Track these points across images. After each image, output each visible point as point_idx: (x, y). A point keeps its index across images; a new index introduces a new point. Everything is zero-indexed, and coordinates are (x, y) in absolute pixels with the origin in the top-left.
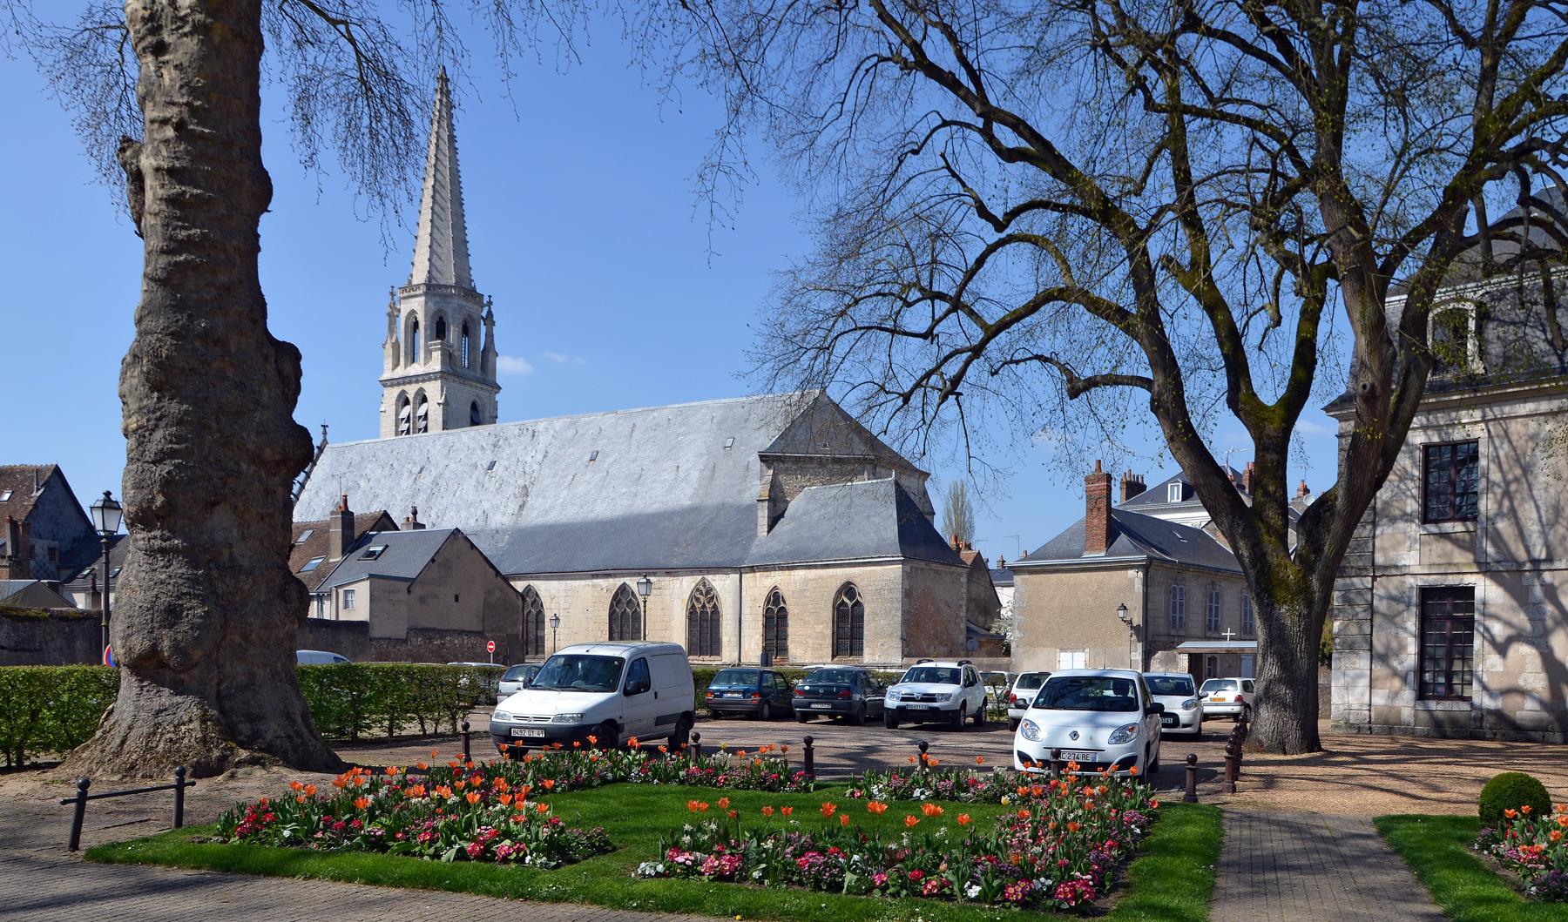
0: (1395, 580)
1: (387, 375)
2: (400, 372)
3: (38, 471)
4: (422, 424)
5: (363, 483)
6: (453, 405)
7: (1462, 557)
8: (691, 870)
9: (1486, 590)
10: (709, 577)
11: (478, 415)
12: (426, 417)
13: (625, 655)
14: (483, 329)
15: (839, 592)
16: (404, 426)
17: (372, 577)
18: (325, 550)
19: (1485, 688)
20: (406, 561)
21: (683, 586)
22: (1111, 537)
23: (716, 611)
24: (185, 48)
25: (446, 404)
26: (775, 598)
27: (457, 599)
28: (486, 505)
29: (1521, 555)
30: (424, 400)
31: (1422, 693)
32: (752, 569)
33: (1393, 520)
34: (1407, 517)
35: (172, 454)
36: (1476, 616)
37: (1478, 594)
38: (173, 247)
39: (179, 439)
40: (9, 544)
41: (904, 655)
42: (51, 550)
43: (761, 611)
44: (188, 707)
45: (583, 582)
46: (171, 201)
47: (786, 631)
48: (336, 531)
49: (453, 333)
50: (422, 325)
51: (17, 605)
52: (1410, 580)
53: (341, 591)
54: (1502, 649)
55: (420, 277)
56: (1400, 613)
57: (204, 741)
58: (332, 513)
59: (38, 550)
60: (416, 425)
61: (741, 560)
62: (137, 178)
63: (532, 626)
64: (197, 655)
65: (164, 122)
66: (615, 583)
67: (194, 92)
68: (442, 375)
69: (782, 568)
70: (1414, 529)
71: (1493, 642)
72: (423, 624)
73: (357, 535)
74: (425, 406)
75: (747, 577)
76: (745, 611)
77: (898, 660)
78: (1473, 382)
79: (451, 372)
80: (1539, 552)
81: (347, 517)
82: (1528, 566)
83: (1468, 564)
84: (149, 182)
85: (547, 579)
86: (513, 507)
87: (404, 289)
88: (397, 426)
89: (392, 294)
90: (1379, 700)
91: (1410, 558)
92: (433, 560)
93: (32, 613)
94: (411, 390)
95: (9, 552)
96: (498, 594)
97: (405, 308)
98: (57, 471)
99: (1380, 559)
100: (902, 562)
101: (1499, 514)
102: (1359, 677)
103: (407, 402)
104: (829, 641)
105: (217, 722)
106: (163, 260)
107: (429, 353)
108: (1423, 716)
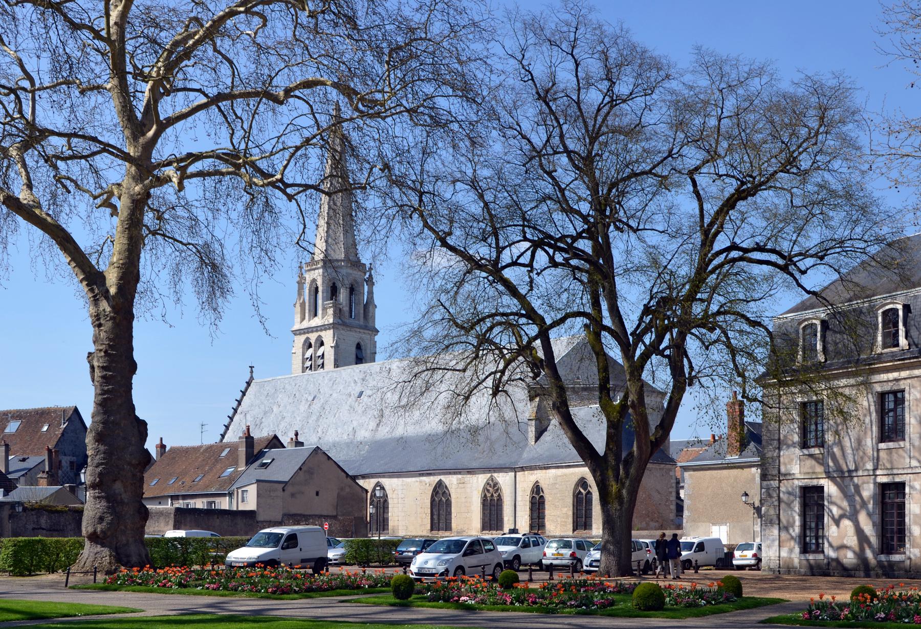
0: (790, 481)
1: (297, 326)
2: (306, 324)
3: (64, 411)
4: (320, 362)
6: (342, 347)
7: (819, 469)
8: (208, 588)
9: (831, 489)
10: (495, 475)
11: (361, 355)
12: (323, 356)
13: (285, 533)
14: (366, 288)
15: (577, 485)
16: (308, 364)
17: (258, 481)
18: (236, 463)
19: (831, 545)
20: (283, 467)
21: (480, 480)
22: (743, 446)
23: (500, 499)
24: (108, 325)
25: (336, 347)
26: (537, 489)
27: (317, 494)
28: (355, 424)
29: (845, 469)
30: (322, 344)
31: (805, 549)
32: (523, 469)
33: (788, 446)
34: (793, 445)
35: (102, 464)
36: (826, 503)
37: (826, 489)
38: (104, 392)
39: (104, 459)
40: (47, 463)
42: (72, 463)
43: (528, 499)
44: (106, 552)
45: (414, 479)
47: (544, 513)
48: (242, 450)
49: (343, 295)
50: (320, 289)
51: (51, 504)
52: (796, 482)
53: (240, 491)
54: (837, 522)
55: (319, 256)
56: (793, 502)
57: (110, 563)
58: (240, 438)
59: (64, 463)
60: (314, 364)
61: (516, 463)
62: (92, 367)
64: (109, 533)
65: (101, 350)
66: (435, 479)
67: (110, 340)
69: (541, 468)
70: (797, 451)
71: (833, 518)
72: (293, 511)
73: (256, 451)
74: (322, 349)
75: (519, 474)
76: (518, 499)
77: (571, 533)
78: (820, 366)
79: (341, 323)
80: (852, 467)
81: (249, 440)
82: (846, 474)
83: (821, 473)
84: (96, 370)
85: (390, 477)
86: (372, 425)
87: (308, 264)
88: (303, 363)
89: (301, 267)
90: (784, 554)
91: (795, 469)
92: (300, 469)
93: (59, 508)
94: (313, 337)
95: (47, 469)
96: (347, 490)
97: (309, 277)
98: (76, 410)
99: (783, 470)
101: (834, 443)
102: (773, 541)
103: (310, 346)
104: (570, 520)
105: (115, 557)
106: (100, 397)
108: (805, 562)
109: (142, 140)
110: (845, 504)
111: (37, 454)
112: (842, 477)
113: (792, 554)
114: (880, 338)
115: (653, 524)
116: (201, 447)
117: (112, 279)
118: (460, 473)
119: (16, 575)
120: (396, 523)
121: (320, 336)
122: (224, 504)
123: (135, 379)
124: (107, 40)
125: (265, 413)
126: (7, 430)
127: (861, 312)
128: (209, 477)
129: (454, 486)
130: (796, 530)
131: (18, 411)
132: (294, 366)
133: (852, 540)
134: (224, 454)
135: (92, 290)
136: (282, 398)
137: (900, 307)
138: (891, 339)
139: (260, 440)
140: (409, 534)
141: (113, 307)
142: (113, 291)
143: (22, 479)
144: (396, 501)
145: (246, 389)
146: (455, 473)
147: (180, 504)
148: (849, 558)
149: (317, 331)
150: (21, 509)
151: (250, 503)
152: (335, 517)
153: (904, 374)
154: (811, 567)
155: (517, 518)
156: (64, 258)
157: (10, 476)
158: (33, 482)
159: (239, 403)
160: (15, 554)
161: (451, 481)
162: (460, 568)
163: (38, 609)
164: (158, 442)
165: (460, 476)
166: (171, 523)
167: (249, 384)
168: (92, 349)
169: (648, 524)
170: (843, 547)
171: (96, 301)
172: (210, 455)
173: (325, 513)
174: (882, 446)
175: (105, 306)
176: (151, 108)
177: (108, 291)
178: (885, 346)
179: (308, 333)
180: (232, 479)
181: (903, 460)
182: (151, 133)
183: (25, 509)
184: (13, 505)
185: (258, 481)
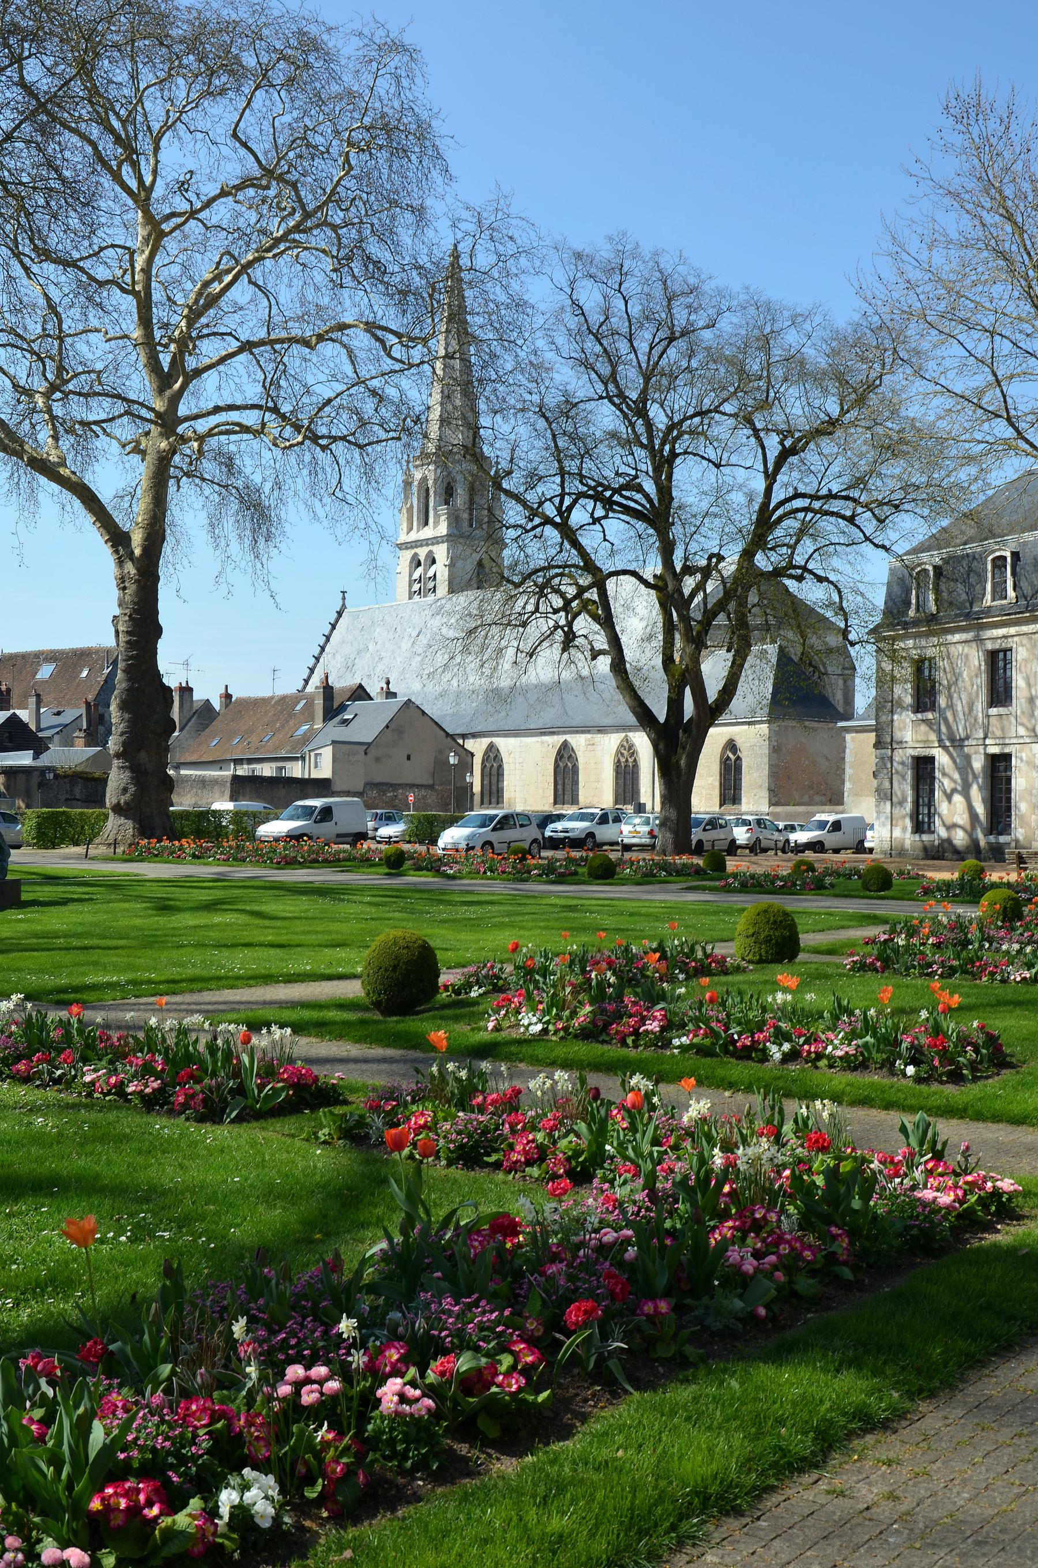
1: (403, 538)
2: (413, 536)
4: (431, 585)
5: (371, 647)
10: (631, 734)
15: (725, 748)
18: (311, 719)
20: (366, 724)
24: (132, 588)
25: (451, 566)
27: (409, 758)
31: (919, 828)
36: (937, 774)
41: (771, 804)
46: (127, 642)
48: (319, 702)
62: (117, 632)
63: (494, 779)
66: (559, 739)
67: (135, 604)
68: (451, 538)
71: (945, 792)
72: (378, 779)
73: (336, 705)
74: (433, 568)
78: (932, 619)
81: (328, 690)
85: (506, 736)
88: (410, 586)
92: (387, 727)
93: (97, 775)
94: (422, 552)
100: (769, 722)
103: (419, 564)
104: (717, 792)
107: (437, 516)
109: (168, 393)
110: (956, 776)
111: (77, 706)
112: (956, 743)
113: (904, 835)
114: (989, 586)
115: (817, 798)
116: (272, 698)
117: (137, 539)
118: (589, 732)
119: (39, 848)
120: (512, 795)
121: (431, 552)
122: (295, 770)
123: (161, 644)
124: (133, 292)
125: (359, 652)
126: (38, 676)
127: (974, 558)
128: (280, 736)
129: (582, 749)
130: (909, 806)
131: (52, 651)
132: (398, 590)
133: (961, 817)
134: (298, 707)
135: (117, 552)
136: (379, 632)
137: (1008, 554)
138: (999, 592)
139: (342, 689)
140: (528, 808)
141: (137, 569)
142: (137, 552)
143: (56, 738)
144: (512, 766)
145: (337, 621)
146: (583, 732)
147: (242, 771)
148: (960, 838)
149: (427, 545)
150: (52, 776)
151: (324, 770)
152: (431, 787)
153: (1013, 630)
154: (925, 849)
155: (598, 789)
156: (90, 519)
157: (40, 734)
158: (69, 742)
159: (328, 638)
160: (39, 826)
161: (578, 742)
162: (489, 843)
163: (53, 873)
164: (223, 691)
165: (589, 736)
166: (228, 793)
167: (340, 614)
168: (117, 611)
169: (811, 798)
170: (955, 826)
171: (120, 563)
172: (282, 708)
173: (418, 782)
174: (993, 711)
175: (130, 568)
176: (177, 362)
177: (132, 552)
178: (993, 600)
179: (416, 547)
180: (306, 739)
181: (1013, 730)
182: (177, 386)
183: (56, 776)
184: (42, 771)
185: (334, 742)
